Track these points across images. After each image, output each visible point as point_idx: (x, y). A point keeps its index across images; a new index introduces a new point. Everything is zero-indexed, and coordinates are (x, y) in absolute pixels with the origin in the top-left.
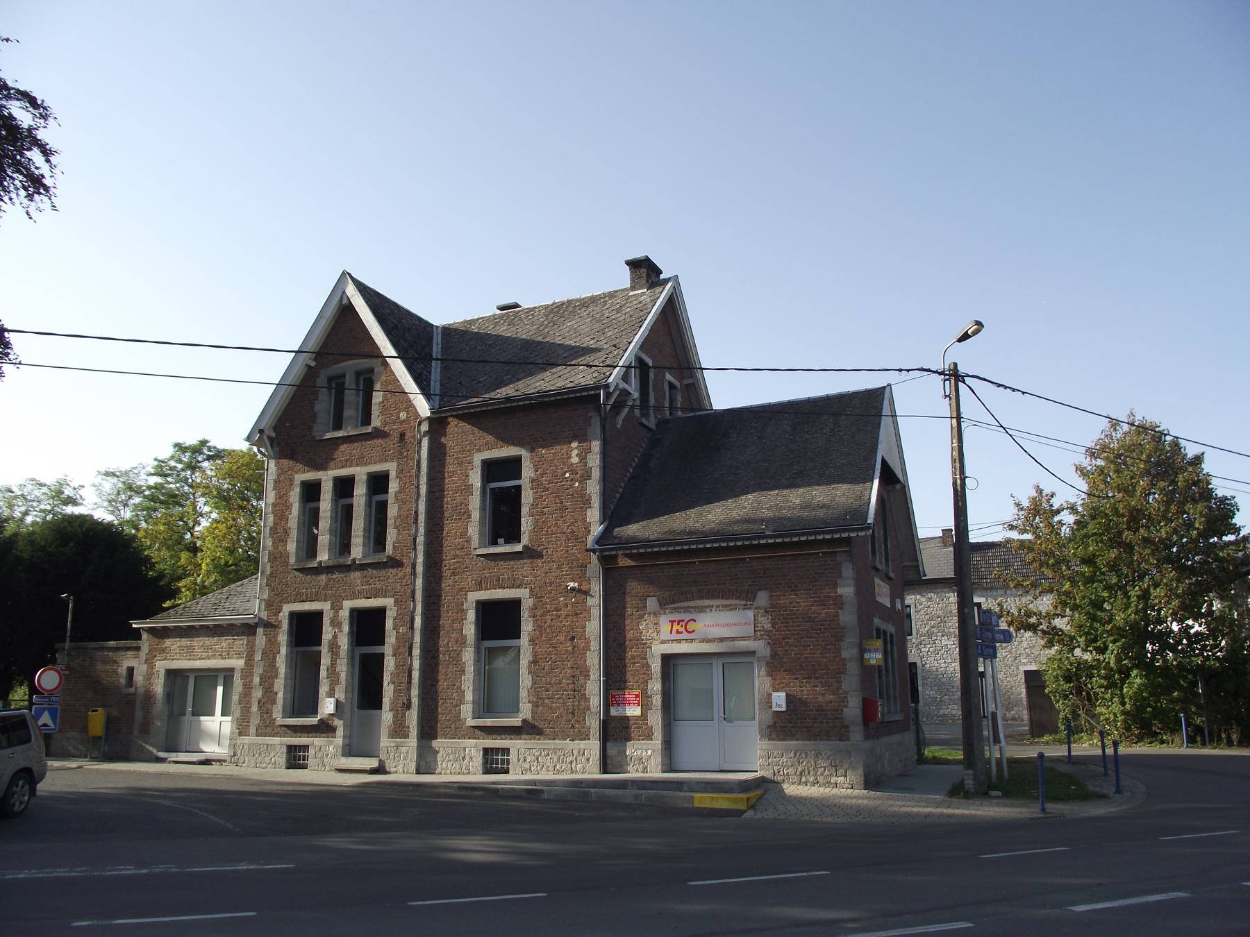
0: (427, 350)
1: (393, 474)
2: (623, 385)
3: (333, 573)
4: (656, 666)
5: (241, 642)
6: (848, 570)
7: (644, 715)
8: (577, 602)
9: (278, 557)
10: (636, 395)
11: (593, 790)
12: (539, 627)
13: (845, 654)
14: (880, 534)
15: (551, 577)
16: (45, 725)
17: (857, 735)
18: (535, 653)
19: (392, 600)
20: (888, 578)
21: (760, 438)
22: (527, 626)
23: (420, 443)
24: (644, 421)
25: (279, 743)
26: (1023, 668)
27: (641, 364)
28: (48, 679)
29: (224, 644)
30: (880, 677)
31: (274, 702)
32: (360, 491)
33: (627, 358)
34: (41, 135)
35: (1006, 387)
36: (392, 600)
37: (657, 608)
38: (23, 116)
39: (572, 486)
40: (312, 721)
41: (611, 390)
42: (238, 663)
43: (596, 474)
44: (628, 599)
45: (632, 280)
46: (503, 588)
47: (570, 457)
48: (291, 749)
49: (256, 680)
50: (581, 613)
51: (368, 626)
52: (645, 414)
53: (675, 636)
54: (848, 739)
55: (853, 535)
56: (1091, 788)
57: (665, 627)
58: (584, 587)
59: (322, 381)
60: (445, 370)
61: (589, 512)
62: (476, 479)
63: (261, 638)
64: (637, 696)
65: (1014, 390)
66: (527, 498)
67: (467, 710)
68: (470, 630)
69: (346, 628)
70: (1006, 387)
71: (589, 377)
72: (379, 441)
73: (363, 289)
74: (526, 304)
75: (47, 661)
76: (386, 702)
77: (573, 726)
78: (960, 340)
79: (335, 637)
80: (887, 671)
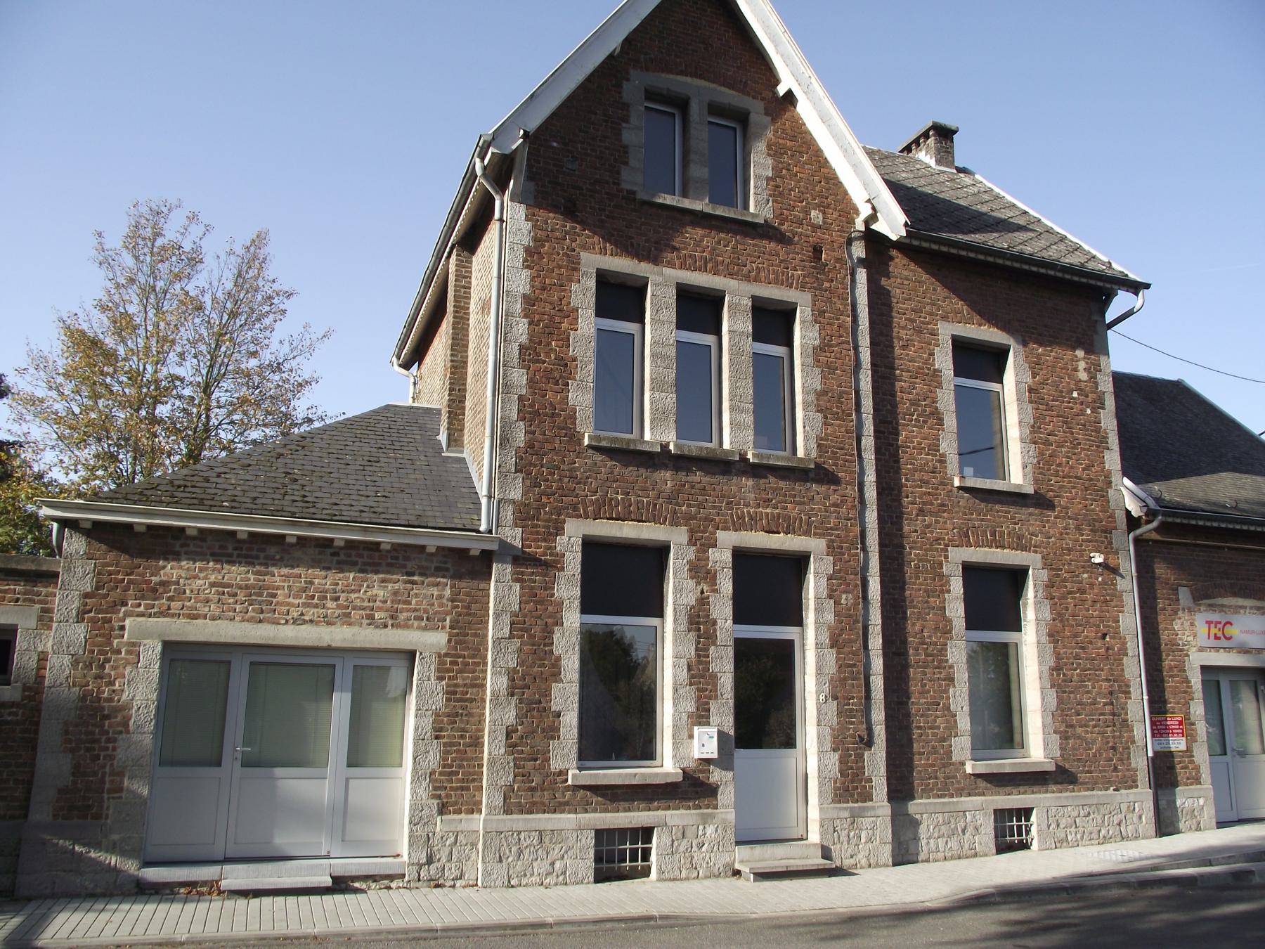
3: (689, 471)
4: (1196, 680)
5: (436, 592)
7: (1189, 749)
8: (1104, 583)
12: (1059, 615)
15: (1068, 542)
18: (1058, 657)
23: (853, 275)
25: (576, 828)
29: (379, 592)
31: (552, 732)
32: (735, 323)
39: (1082, 413)
44: (1158, 586)
46: (1003, 547)
48: (1001, 815)
50: (1111, 600)
51: (768, 586)
53: (1212, 642)
57: (1202, 629)
58: (1111, 563)
63: (501, 590)
67: (961, 746)
68: (956, 610)
69: (726, 585)
72: (770, 246)
77: (1116, 769)
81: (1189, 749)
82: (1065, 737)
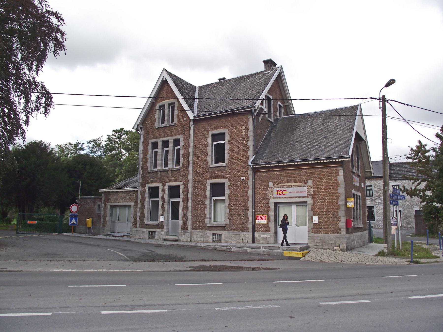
0: (193, 95)
1: (181, 139)
2: (260, 106)
6: (341, 172)
7: (268, 224)
9: (145, 168)
10: (266, 110)
11: (249, 249)
13: (340, 203)
14: (355, 159)
16: (73, 223)
17: (343, 232)
18: (230, 202)
19: (182, 183)
20: (359, 176)
21: (311, 124)
22: (227, 192)
24: (269, 119)
26: (415, 209)
27: (268, 99)
28: (74, 208)
30: (354, 211)
33: (263, 96)
34: (60, 27)
35: (404, 104)
36: (182, 183)
37: (273, 186)
38: (54, 20)
40: (156, 223)
41: (256, 108)
42: (133, 204)
43: (251, 138)
45: (265, 68)
47: (242, 132)
49: (138, 209)
52: (270, 116)
54: (340, 234)
55: (343, 160)
56: (433, 254)
59: (157, 107)
60: (199, 102)
61: (249, 152)
62: (209, 140)
64: (265, 217)
65: (408, 105)
66: (227, 147)
68: (208, 193)
69: (167, 192)
70: (404, 104)
71: (249, 104)
73: (170, 74)
74: (228, 78)
75: (74, 202)
76: (180, 217)
78: (387, 85)
79: (163, 195)
80: (357, 209)
81: (268, 224)
82: (230, 219)
